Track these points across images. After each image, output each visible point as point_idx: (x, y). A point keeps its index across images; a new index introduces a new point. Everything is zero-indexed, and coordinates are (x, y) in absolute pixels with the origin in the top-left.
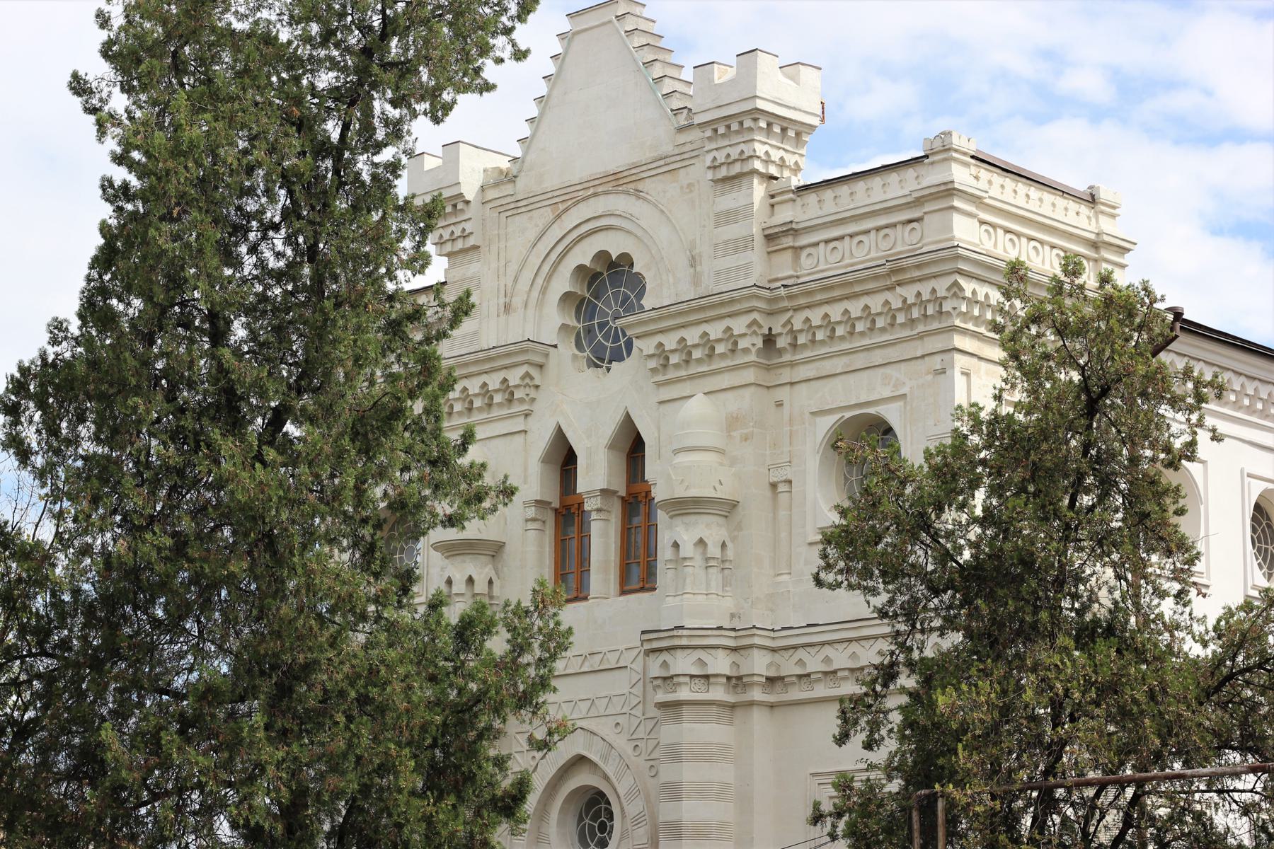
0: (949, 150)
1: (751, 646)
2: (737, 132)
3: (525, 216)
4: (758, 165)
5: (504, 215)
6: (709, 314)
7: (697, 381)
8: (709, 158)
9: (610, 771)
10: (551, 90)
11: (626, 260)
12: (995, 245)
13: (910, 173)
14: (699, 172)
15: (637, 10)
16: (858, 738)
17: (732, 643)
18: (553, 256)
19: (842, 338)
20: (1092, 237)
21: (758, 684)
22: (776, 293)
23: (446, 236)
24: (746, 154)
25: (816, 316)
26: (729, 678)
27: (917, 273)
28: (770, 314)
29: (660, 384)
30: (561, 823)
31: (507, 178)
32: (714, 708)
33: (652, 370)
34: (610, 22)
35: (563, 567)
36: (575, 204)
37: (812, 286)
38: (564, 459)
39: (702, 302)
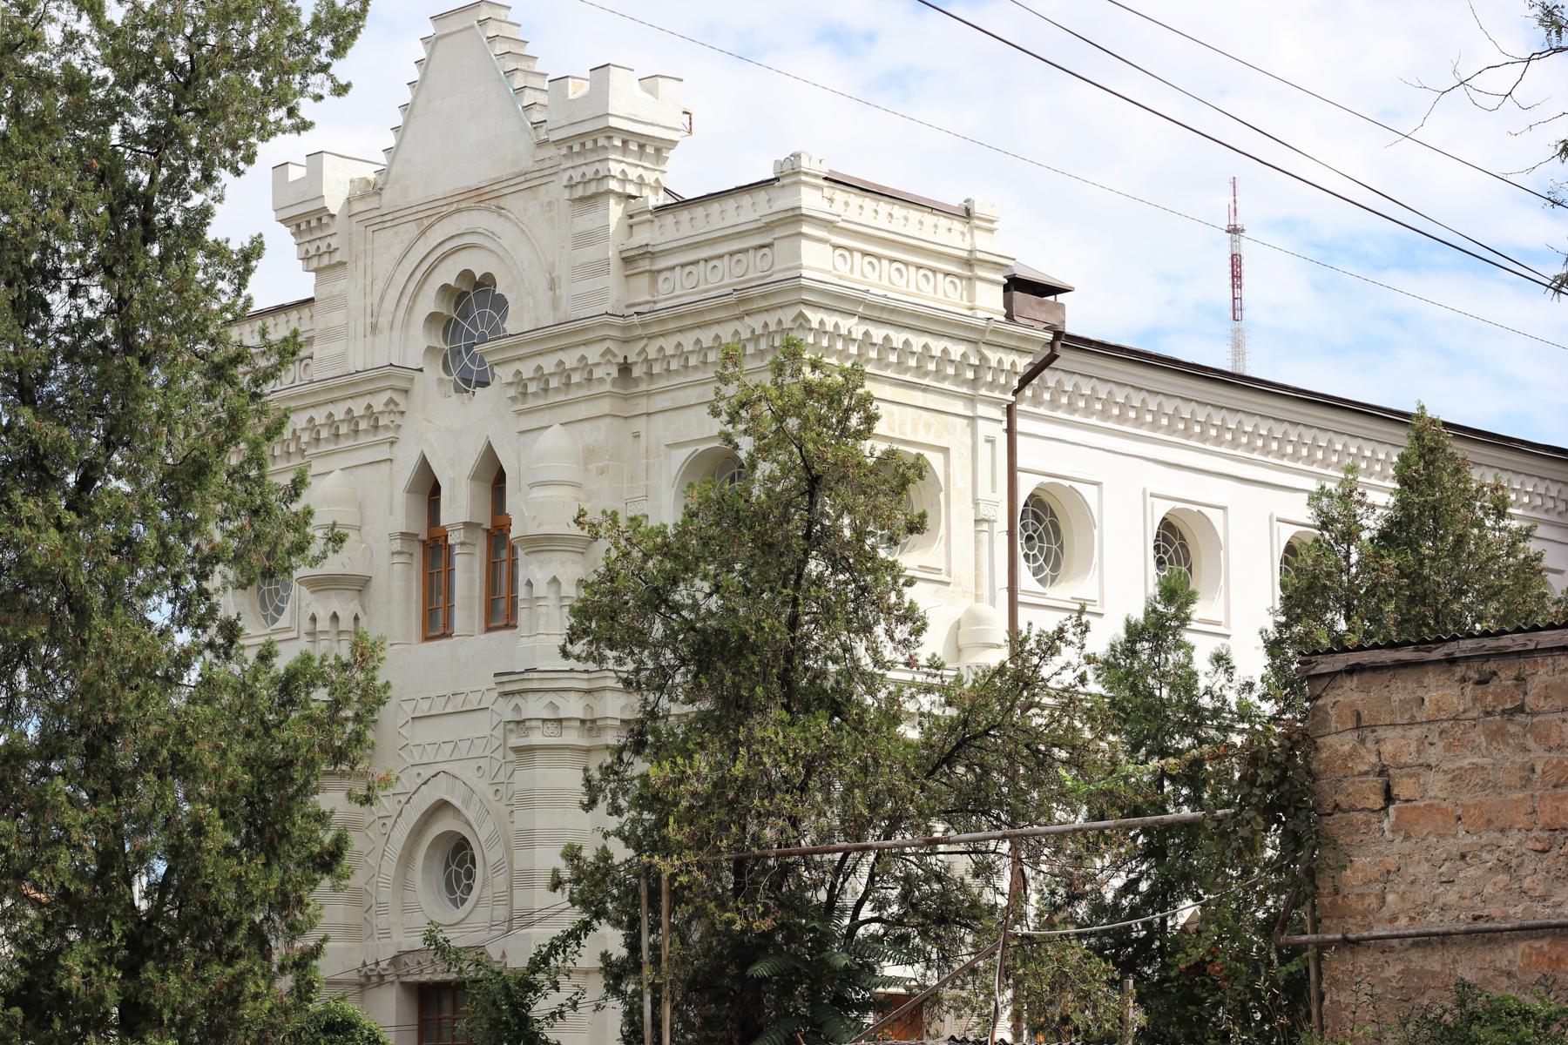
0: (798, 173)
1: (604, 689)
2: (592, 150)
3: (391, 232)
4: (614, 185)
5: (370, 229)
6: (564, 342)
7: (555, 411)
8: (566, 176)
9: (470, 815)
10: (415, 97)
11: (488, 281)
12: (852, 269)
13: (762, 196)
14: (556, 190)
15: (502, 14)
16: (602, 806)
17: (585, 686)
18: (418, 275)
19: (695, 368)
20: (965, 254)
21: (613, 727)
22: (629, 320)
23: (312, 252)
24: (601, 174)
25: (669, 345)
26: (583, 722)
27: (764, 304)
28: (626, 342)
29: (520, 413)
30: (426, 869)
31: (373, 190)
32: (568, 753)
33: (511, 398)
34: (472, 27)
35: (431, 603)
36: (442, 218)
37: (663, 314)
38: (429, 489)
39: (556, 330)
